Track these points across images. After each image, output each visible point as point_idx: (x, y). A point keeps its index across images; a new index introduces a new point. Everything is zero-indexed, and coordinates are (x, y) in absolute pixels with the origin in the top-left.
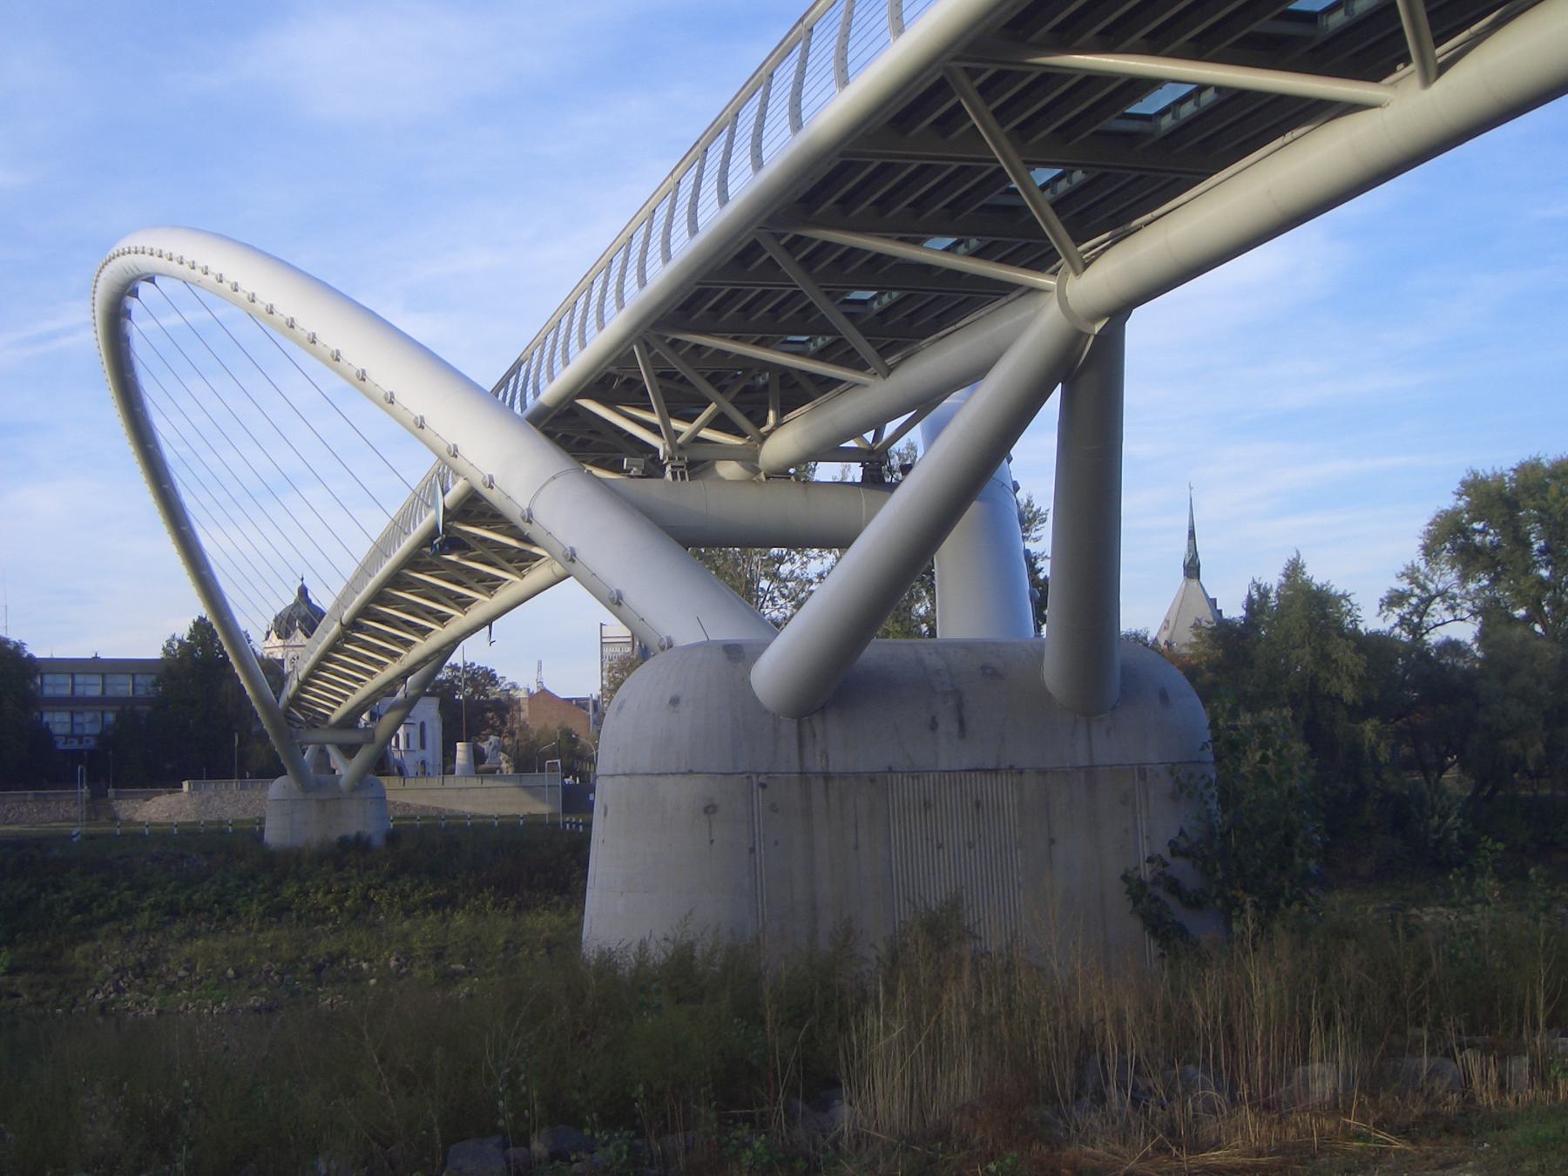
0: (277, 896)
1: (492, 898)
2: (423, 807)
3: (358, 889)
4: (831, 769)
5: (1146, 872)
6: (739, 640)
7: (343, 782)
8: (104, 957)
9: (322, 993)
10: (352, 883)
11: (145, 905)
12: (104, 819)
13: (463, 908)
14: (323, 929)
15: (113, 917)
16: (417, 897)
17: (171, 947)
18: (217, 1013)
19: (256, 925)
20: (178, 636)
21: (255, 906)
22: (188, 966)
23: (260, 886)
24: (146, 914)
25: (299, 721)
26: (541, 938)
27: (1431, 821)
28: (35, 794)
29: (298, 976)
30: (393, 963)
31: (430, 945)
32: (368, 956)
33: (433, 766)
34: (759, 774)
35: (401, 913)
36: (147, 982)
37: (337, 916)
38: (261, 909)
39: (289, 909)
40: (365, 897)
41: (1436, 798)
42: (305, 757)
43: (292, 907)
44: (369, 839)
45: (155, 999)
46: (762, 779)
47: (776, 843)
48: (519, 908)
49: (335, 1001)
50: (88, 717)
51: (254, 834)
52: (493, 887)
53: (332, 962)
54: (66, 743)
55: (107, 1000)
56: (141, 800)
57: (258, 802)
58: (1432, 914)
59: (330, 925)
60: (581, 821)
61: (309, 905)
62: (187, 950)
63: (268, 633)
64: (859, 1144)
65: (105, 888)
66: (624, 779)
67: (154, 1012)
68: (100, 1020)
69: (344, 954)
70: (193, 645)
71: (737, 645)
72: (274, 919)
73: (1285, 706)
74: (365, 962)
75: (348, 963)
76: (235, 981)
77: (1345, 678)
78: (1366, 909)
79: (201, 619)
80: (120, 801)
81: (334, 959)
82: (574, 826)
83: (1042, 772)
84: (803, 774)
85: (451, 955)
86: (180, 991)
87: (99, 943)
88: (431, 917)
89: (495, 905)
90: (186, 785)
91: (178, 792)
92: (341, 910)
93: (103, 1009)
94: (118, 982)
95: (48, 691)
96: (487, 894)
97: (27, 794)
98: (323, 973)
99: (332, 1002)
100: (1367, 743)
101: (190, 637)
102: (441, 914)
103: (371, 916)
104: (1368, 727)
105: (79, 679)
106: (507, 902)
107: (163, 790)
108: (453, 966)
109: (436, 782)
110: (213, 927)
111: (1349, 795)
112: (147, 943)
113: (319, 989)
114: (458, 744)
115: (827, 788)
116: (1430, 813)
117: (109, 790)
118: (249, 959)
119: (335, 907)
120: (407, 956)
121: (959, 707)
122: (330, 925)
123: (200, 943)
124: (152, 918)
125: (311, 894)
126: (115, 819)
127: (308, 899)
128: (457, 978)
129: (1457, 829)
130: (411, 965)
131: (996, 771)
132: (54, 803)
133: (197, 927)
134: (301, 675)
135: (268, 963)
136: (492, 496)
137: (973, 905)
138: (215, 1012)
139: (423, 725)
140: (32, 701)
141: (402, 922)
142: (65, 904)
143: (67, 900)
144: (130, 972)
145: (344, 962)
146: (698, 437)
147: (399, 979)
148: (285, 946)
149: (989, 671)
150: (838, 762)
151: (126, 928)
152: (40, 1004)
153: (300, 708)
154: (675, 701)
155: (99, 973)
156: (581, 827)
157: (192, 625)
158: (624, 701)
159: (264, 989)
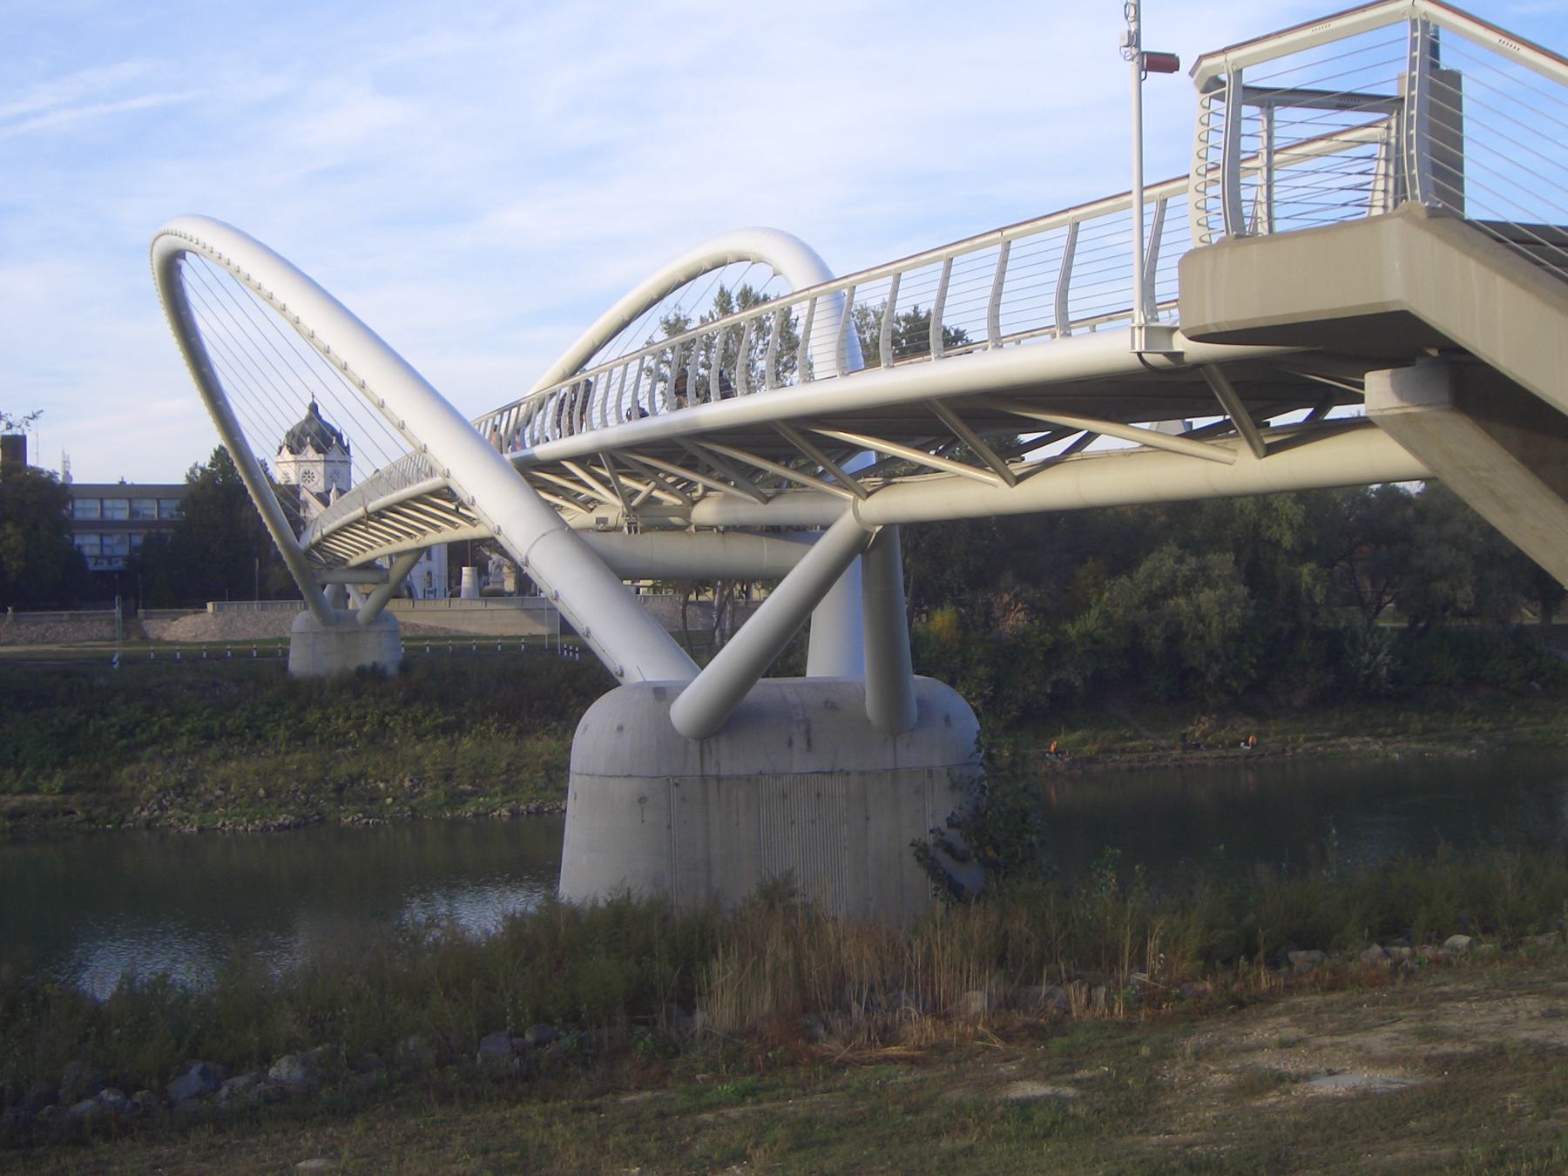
0: (301, 722)
1: (496, 724)
2: (431, 628)
3: (375, 715)
4: (722, 773)
5: (930, 839)
6: (663, 682)
7: (360, 617)
8: (148, 778)
9: (344, 811)
10: (369, 710)
11: (184, 730)
12: (134, 638)
13: (470, 732)
14: (344, 752)
15: (154, 741)
16: (427, 723)
17: (208, 768)
18: (251, 830)
19: (283, 749)
20: (201, 464)
21: (281, 731)
22: (223, 786)
23: (286, 713)
24: (185, 739)
25: (320, 563)
26: (541, 761)
27: (1362, 657)
28: (72, 615)
29: (323, 795)
30: (407, 784)
31: (440, 767)
32: (384, 777)
34: (674, 778)
35: (414, 737)
36: (188, 801)
37: (356, 741)
38: (288, 733)
39: (312, 734)
40: (381, 722)
41: (1368, 636)
42: (325, 592)
43: (316, 731)
44: (384, 668)
45: (195, 817)
46: (676, 780)
48: (520, 733)
49: (356, 818)
50: (116, 538)
51: (275, 655)
52: (497, 714)
53: (352, 783)
54: (96, 564)
55: (152, 817)
56: (168, 620)
57: (277, 622)
58: (1359, 743)
59: (350, 748)
60: (577, 649)
61: (331, 729)
62: (221, 771)
63: (281, 449)
64: (705, 1037)
65: (147, 715)
66: (588, 778)
67: (195, 829)
68: (146, 834)
69: (363, 775)
70: (215, 473)
71: (663, 688)
72: (300, 743)
73: (1228, 551)
74: (382, 782)
75: (367, 783)
76: (266, 800)
77: (1285, 526)
78: (1298, 738)
79: (221, 447)
80: (149, 621)
81: (354, 780)
82: (571, 653)
83: (862, 773)
85: (458, 777)
86: (217, 809)
87: (144, 764)
88: (441, 741)
89: (498, 731)
90: (210, 606)
91: (203, 612)
93: (149, 824)
94: (161, 800)
95: (79, 515)
96: (491, 720)
97: (62, 615)
98: (345, 793)
99: (353, 820)
100: (1304, 584)
101: (212, 465)
102: (450, 739)
103: (387, 740)
104: (1306, 571)
105: (108, 503)
106: (509, 727)
107: (189, 610)
108: (461, 787)
109: (443, 604)
110: (245, 750)
112: (185, 766)
113: (341, 807)
114: (464, 568)
115: (719, 787)
116: (1361, 650)
117: (139, 611)
118: (278, 779)
119: (354, 732)
120: (419, 778)
121: (808, 731)
122: (350, 748)
123: (233, 764)
124: (189, 743)
125: (332, 720)
126: (145, 638)
127: (330, 725)
128: (464, 797)
129: (1387, 665)
130: (424, 786)
131: (831, 773)
132: (88, 623)
133: (230, 751)
134: (325, 531)
135: (295, 783)
136: (501, 539)
137: (800, 875)
138: (249, 829)
140: (67, 526)
141: (415, 745)
142: (112, 730)
143: (113, 726)
144: (172, 792)
145: (363, 782)
146: (652, 496)
147: (412, 797)
148: (310, 768)
149: (829, 705)
150: (725, 770)
152: (90, 820)
153: (320, 551)
154: (620, 728)
155: (144, 792)
156: (577, 655)
157: (213, 453)
158: (587, 725)
159: (292, 808)
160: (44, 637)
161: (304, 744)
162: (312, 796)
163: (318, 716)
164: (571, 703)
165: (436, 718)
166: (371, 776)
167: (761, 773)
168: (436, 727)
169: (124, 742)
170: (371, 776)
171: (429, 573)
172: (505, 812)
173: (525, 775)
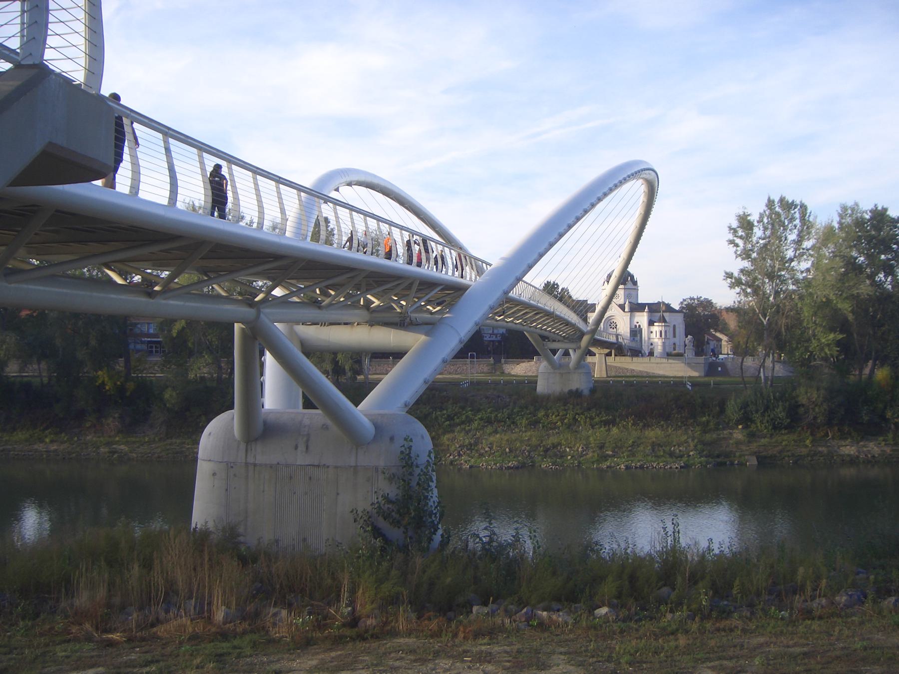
2: (640, 371)
4: (257, 462)
11: (477, 418)
12: (498, 373)
15: (463, 423)
23: (528, 412)
26: (650, 441)
30: (580, 449)
31: (598, 442)
33: (680, 346)
34: (231, 463)
40: (574, 418)
45: (473, 460)
46: (232, 465)
47: (235, 488)
48: (644, 426)
53: (553, 448)
62: (491, 439)
68: (451, 467)
69: (560, 444)
72: (533, 427)
75: (561, 448)
81: (554, 446)
83: (336, 467)
84: (247, 464)
89: (633, 425)
92: (562, 423)
93: (451, 463)
111: (138, 532)
115: (254, 470)
120: (587, 447)
121: (307, 441)
123: (498, 436)
124: (479, 424)
131: (318, 466)
139: (674, 326)
145: (559, 448)
147: (581, 457)
150: (260, 459)
151: (467, 428)
160: (456, 371)
161: (535, 428)
162: (532, 453)
163: (543, 414)
164: (674, 412)
165: (602, 417)
166: (564, 445)
167: (278, 464)
168: (601, 422)
169: (448, 422)
170: (564, 445)
171: (674, 344)
172: (623, 466)
173: (641, 448)
